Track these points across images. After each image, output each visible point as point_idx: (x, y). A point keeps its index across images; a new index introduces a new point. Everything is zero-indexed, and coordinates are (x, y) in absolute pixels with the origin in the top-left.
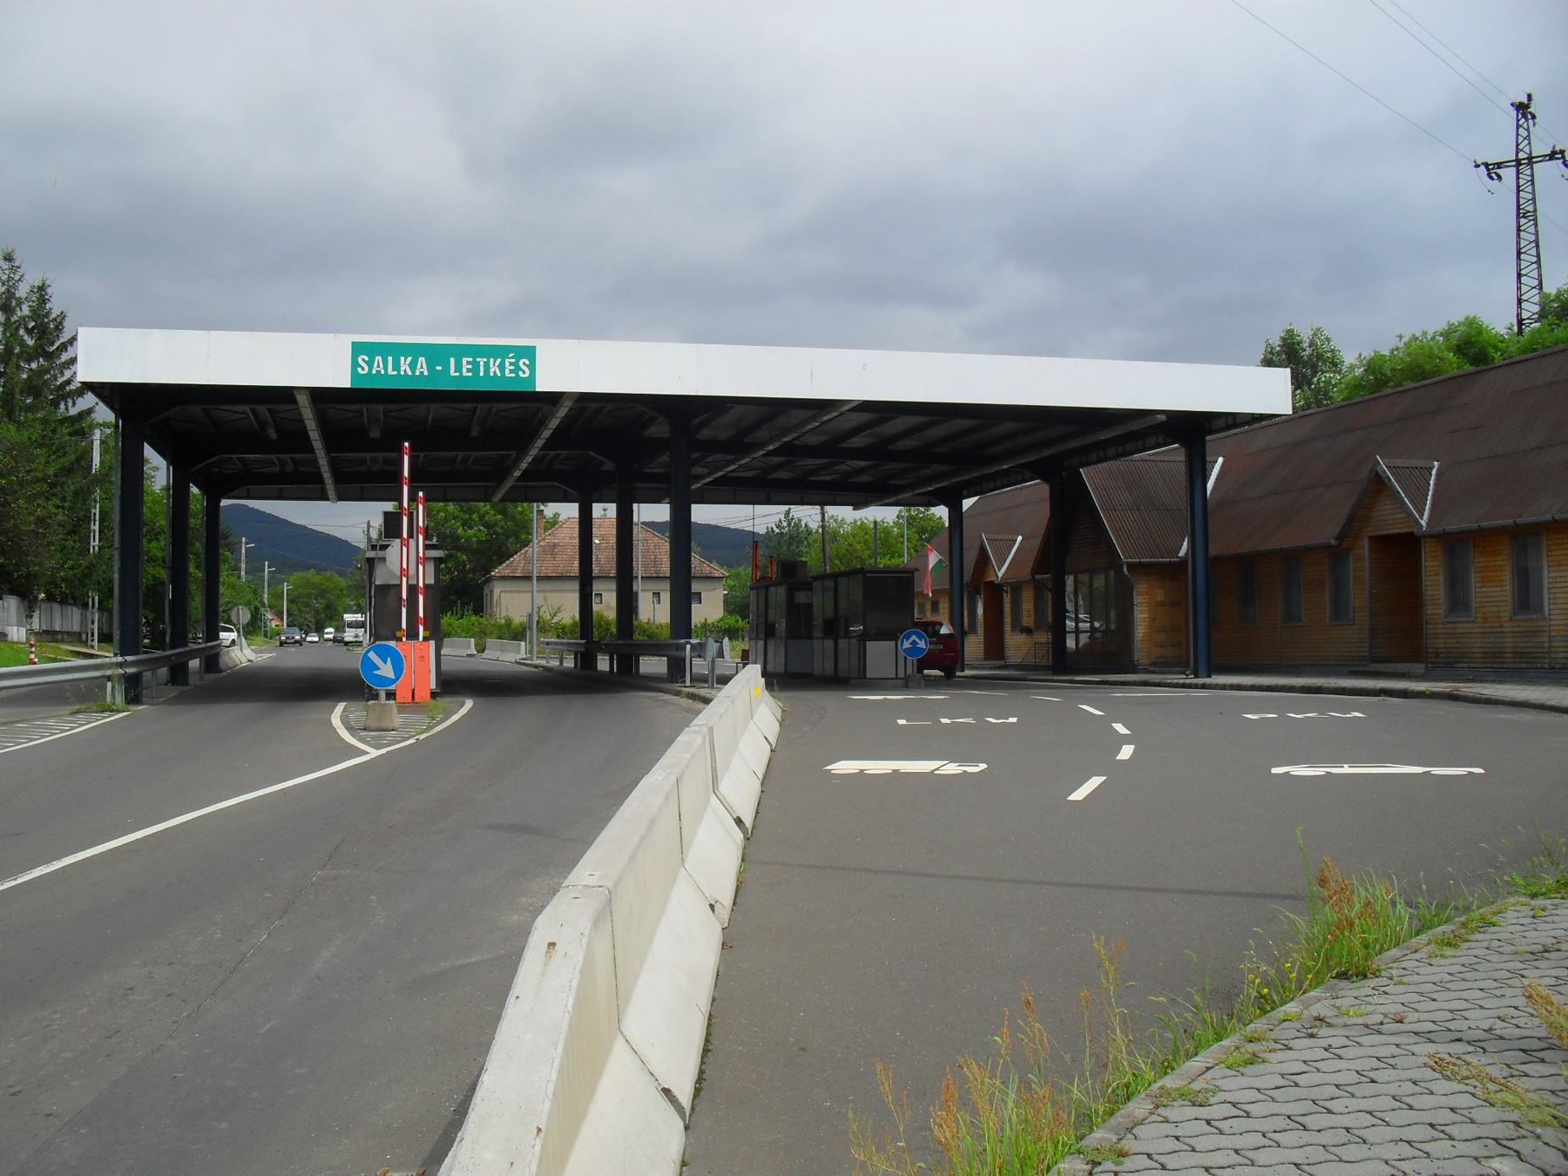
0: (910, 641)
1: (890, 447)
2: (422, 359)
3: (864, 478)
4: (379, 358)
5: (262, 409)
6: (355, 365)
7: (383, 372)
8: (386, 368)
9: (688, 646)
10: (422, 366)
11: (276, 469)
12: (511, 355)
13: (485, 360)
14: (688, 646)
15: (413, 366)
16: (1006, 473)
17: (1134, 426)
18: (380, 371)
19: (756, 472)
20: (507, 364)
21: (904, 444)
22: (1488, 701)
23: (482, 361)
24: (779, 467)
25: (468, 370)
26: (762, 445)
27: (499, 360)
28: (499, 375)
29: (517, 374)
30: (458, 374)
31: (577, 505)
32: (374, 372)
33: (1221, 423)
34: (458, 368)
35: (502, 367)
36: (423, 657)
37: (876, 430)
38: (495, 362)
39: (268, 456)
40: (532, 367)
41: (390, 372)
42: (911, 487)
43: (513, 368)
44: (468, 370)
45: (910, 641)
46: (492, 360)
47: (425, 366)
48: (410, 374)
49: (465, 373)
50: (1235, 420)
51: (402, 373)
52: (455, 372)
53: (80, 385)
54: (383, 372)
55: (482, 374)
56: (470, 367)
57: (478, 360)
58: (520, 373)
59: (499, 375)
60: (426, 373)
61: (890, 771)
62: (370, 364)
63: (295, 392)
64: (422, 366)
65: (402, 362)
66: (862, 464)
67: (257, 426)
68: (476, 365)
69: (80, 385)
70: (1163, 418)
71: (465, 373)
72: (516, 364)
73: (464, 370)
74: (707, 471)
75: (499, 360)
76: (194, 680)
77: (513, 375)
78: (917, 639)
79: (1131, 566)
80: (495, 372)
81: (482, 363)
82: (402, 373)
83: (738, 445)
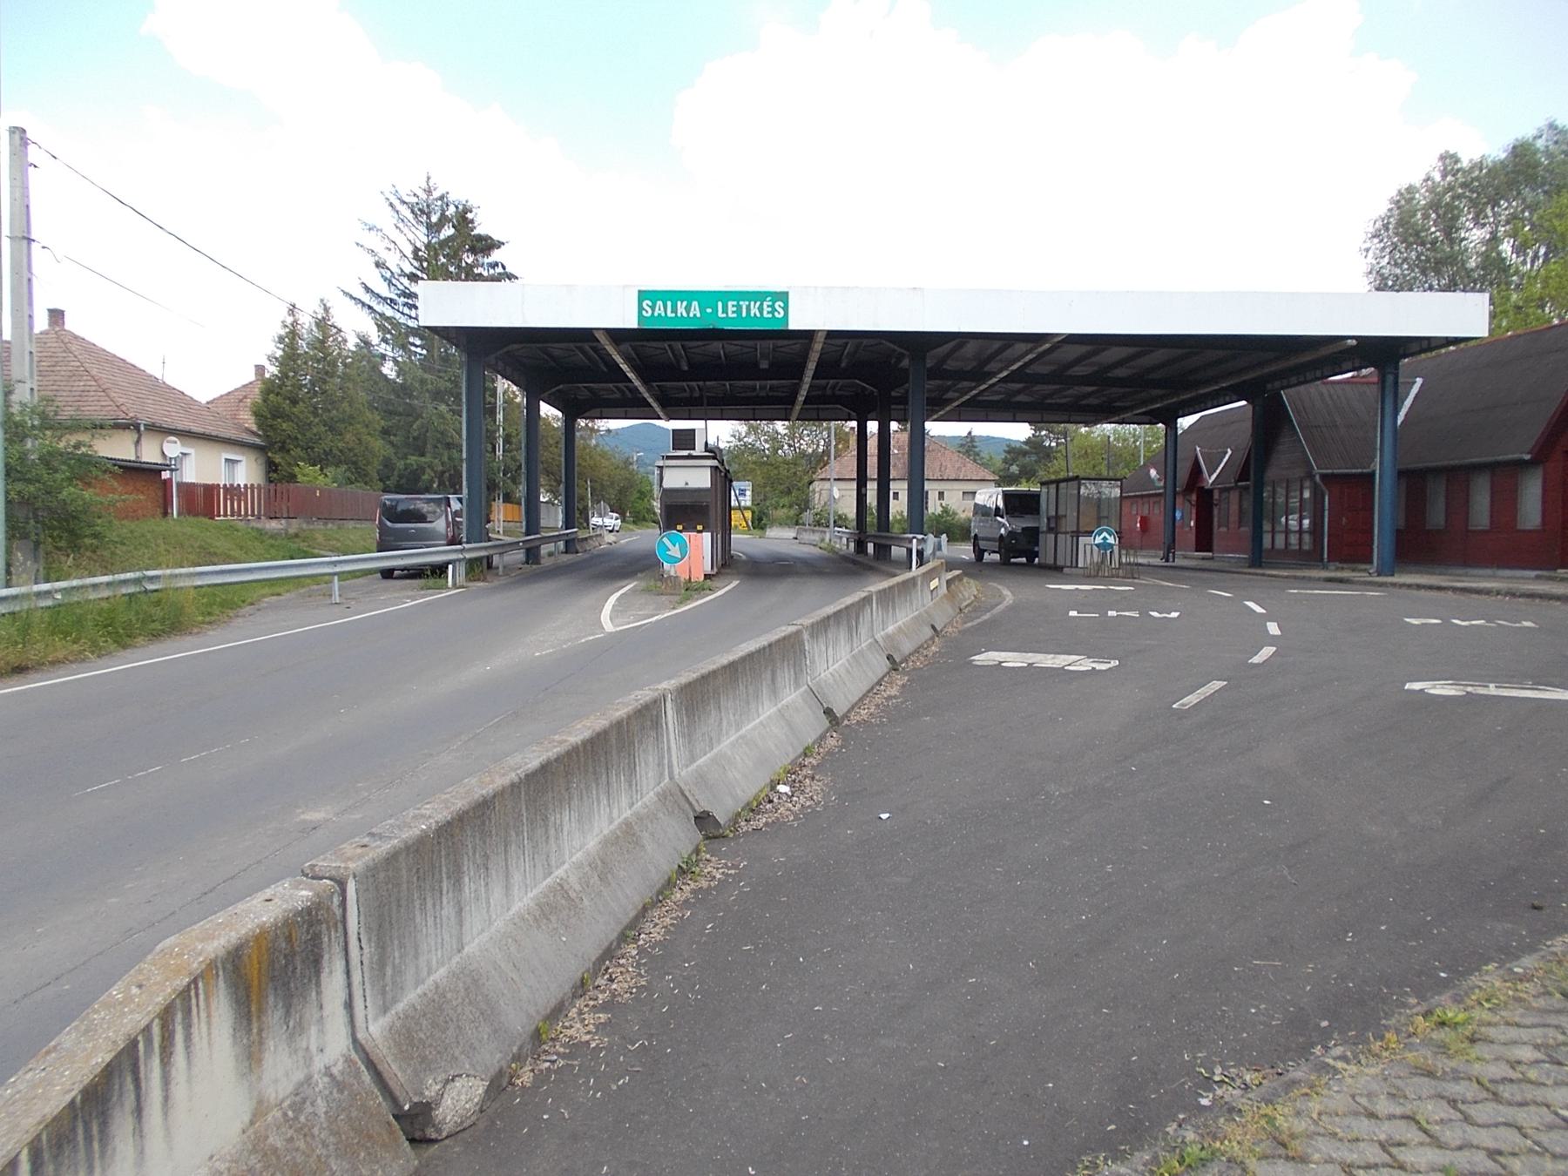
0: (1102, 536)
1: (1109, 375)
2: (695, 304)
3: (1093, 401)
4: (660, 303)
5: (678, 345)
6: (641, 308)
7: (663, 314)
9: (915, 541)
10: (695, 310)
11: (686, 395)
14: (915, 541)
15: (688, 309)
16: (1206, 396)
17: (1325, 351)
19: (1001, 396)
20: (765, 306)
21: (1121, 372)
22: (1478, 592)
23: (744, 304)
24: (1019, 392)
26: (993, 374)
27: (758, 304)
29: (773, 315)
33: (1415, 347)
34: (725, 310)
35: (761, 309)
37: (1094, 359)
39: (680, 383)
40: (786, 309)
41: (670, 314)
42: (1131, 408)
44: (733, 312)
46: (752, 303)
47: (697, 309)
49: (730, 315)
50: (1429, 344)
51: (679, 315)
58: (776, 314)
60: (698, 315)
63: (595, 332)
64: (695, 310)
66: (1090, 389)
67: (586, 361)
68: (739, 307)
70: (1354, 342)
71: (730, 315)
72: (772, 306)
73: (730, 312)
74: (957, 394)
75: (758, 304)
76: (546, 562)
78: (1108, 536)
79: (1323, 476)
81: (744, 307)
83: (979, 374)
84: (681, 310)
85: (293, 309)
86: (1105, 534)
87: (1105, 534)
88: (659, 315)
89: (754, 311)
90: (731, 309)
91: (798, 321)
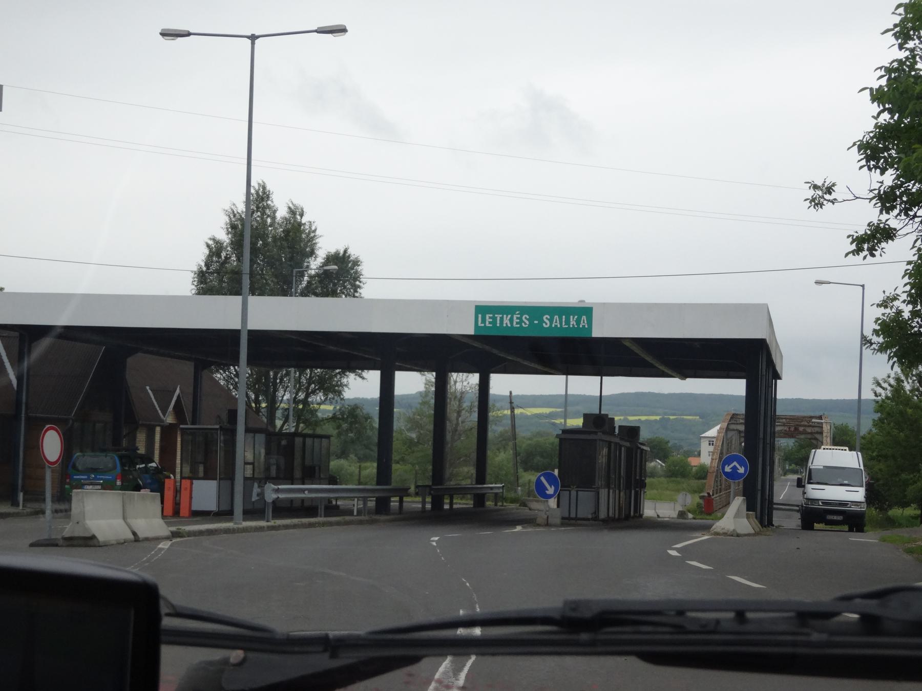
0: (732, 466)
4: (556, 317)
7: (559, 326)
8: (561, 323)
12: (518, 312)
13: (501, 316)
15: (578, 322)
18: (557, 325)
20: (515, 318)
23: (498, 316)
25: (490, 323)
28: (509, 325)
29: (521, 325)
30: (567, 326)
31: (744, 381)
32: (553, 326)
35: (511, 320)
36: (170, 488)
38: (507, 317)
43: (518, 321)
45: (732, 466)
47: (586, 322)
48: (576, 326)
49: (487, 324)
51: (571, 326)
52: (481, 323)
53: (63, 330)
54: (559, 326)
55: (498, 325)
56: (491, 320)
57: (496, 316)
59: (509, 325)
61: (822, 467)
62: (551, 321)
64: (556, 322)
65: (571, 320)
68: (494, 319)
69: (63, 330)
71: (487, 324)
73: (487, 323)
75: (509, 316)
77: (518, 326)
78: (738, 466)
80: (506, 324)
81: (498, 319)
82: (571, 326)
84: (573, 322)
85: (349, 389)
86: (735, 463)
87: (735, 463)
88: (584, 326)
89: (506, 321)
90: (488, 320)
91: (597, 332)
